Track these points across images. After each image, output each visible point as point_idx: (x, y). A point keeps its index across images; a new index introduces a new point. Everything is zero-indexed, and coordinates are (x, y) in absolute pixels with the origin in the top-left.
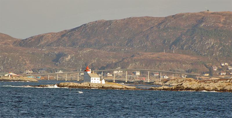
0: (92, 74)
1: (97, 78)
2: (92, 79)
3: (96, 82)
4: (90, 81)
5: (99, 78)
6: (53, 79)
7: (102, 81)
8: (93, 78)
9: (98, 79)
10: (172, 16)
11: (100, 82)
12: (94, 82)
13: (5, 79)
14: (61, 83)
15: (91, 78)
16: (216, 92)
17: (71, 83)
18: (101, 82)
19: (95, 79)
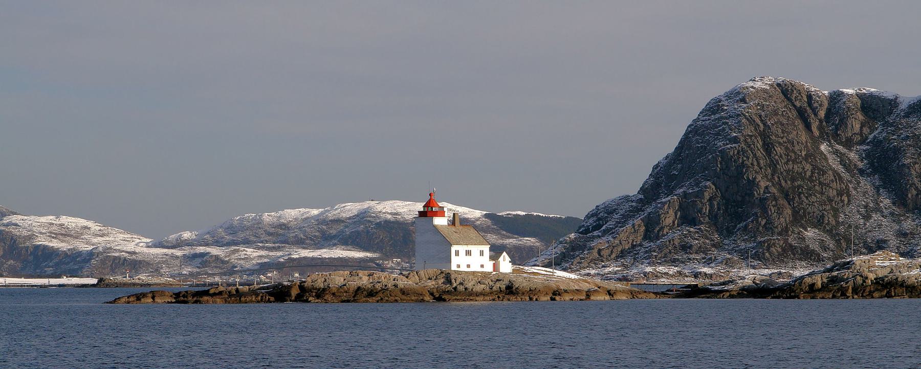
0: (453, 229)
1: (475, 249)
2: (457, 253)
3: (475, 268)
4: (449, 260)
5: (486, 249)
6: (786, 280)
7: (501, 259)
8: (462, 249)
9: (482, 253)
10: (328, 297)
11: (489, 267)
12: (463, 268)
13: (51, 245)
14: (314, 276)
15: (454, 248)
16: (369, 255)
17: (361, 273)
18: (496, 267)
19: (468, 253)
